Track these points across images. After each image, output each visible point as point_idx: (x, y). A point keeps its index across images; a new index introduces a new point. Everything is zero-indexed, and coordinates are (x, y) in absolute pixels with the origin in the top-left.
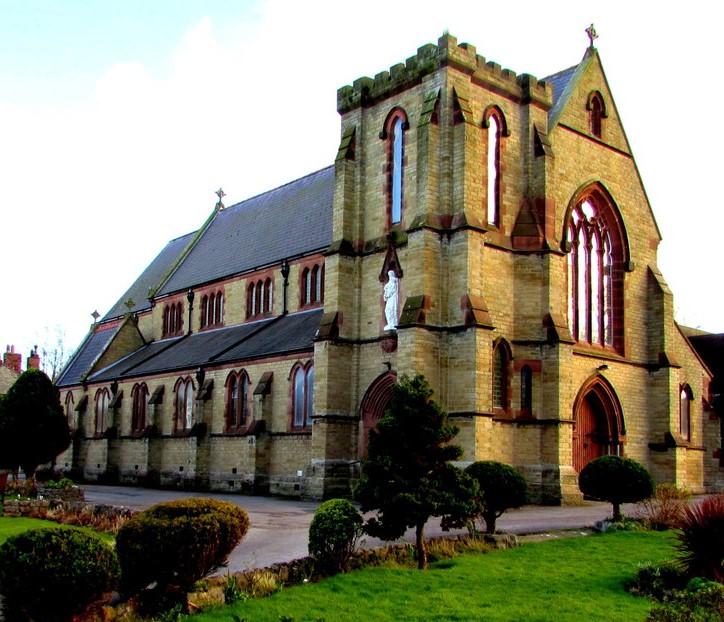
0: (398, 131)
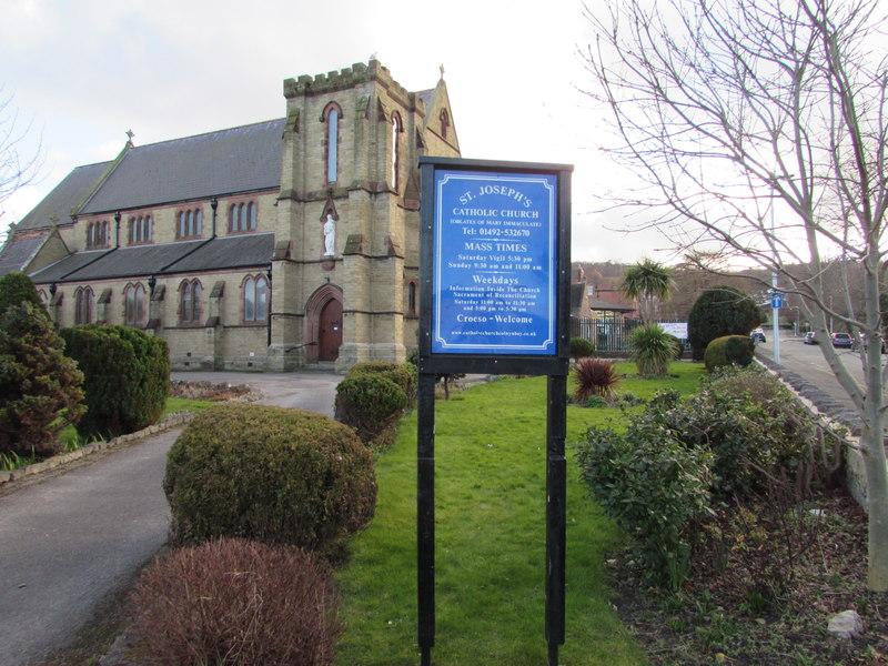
0: (334, 116)
